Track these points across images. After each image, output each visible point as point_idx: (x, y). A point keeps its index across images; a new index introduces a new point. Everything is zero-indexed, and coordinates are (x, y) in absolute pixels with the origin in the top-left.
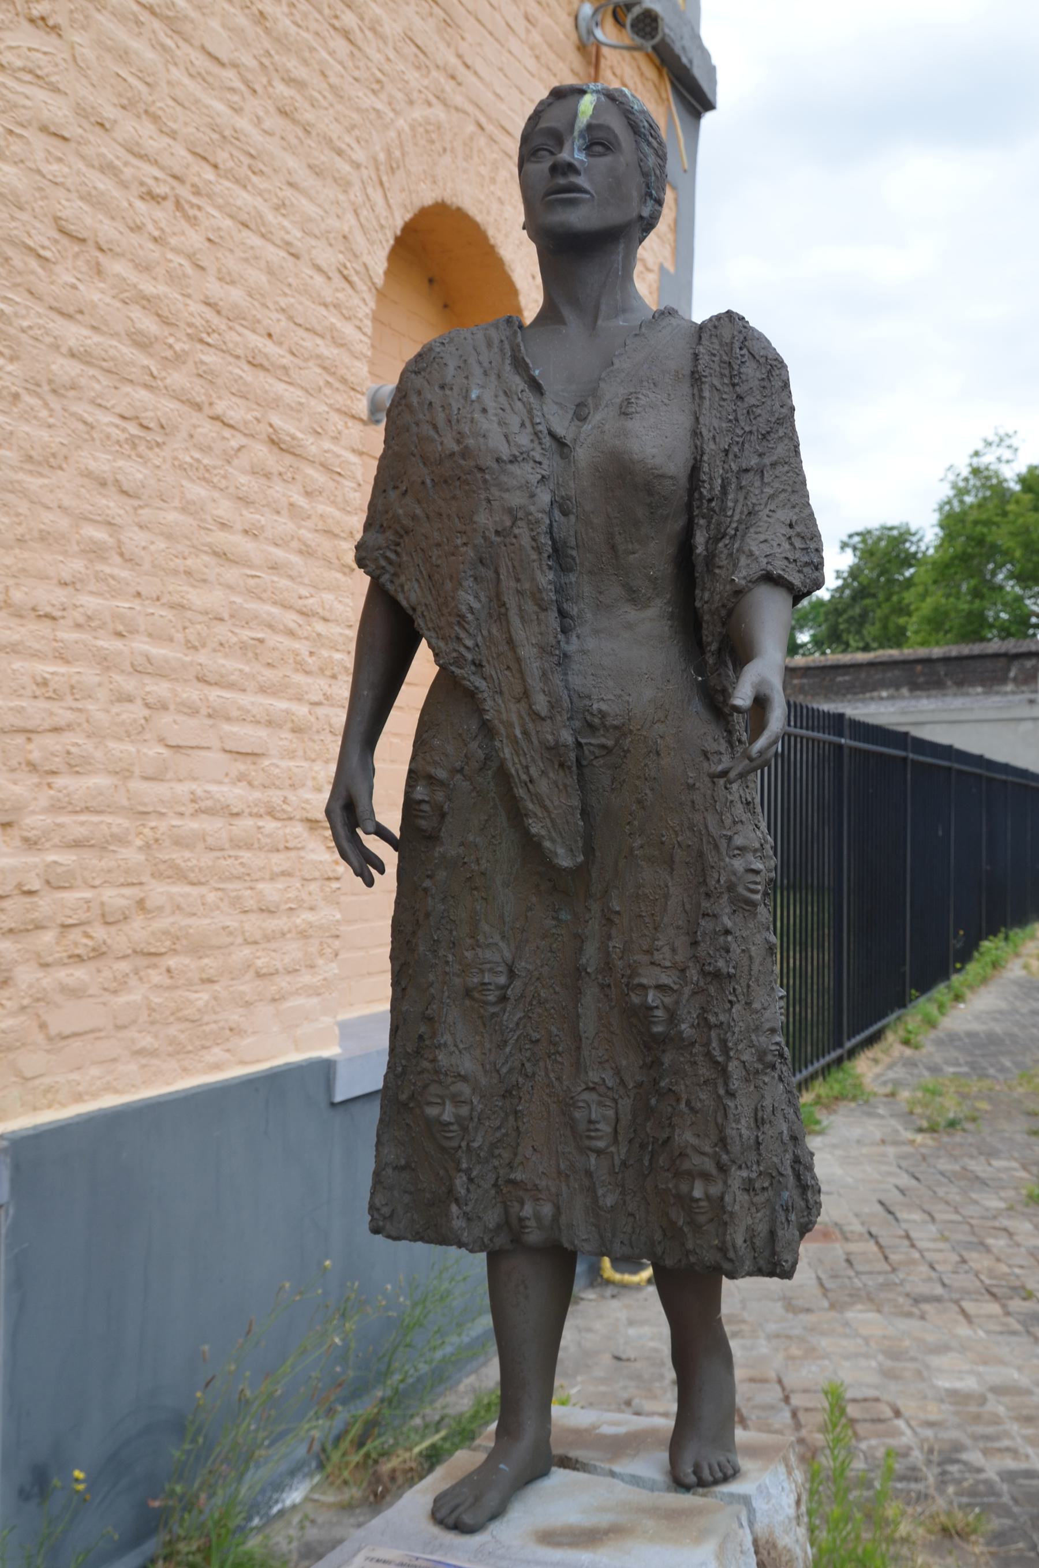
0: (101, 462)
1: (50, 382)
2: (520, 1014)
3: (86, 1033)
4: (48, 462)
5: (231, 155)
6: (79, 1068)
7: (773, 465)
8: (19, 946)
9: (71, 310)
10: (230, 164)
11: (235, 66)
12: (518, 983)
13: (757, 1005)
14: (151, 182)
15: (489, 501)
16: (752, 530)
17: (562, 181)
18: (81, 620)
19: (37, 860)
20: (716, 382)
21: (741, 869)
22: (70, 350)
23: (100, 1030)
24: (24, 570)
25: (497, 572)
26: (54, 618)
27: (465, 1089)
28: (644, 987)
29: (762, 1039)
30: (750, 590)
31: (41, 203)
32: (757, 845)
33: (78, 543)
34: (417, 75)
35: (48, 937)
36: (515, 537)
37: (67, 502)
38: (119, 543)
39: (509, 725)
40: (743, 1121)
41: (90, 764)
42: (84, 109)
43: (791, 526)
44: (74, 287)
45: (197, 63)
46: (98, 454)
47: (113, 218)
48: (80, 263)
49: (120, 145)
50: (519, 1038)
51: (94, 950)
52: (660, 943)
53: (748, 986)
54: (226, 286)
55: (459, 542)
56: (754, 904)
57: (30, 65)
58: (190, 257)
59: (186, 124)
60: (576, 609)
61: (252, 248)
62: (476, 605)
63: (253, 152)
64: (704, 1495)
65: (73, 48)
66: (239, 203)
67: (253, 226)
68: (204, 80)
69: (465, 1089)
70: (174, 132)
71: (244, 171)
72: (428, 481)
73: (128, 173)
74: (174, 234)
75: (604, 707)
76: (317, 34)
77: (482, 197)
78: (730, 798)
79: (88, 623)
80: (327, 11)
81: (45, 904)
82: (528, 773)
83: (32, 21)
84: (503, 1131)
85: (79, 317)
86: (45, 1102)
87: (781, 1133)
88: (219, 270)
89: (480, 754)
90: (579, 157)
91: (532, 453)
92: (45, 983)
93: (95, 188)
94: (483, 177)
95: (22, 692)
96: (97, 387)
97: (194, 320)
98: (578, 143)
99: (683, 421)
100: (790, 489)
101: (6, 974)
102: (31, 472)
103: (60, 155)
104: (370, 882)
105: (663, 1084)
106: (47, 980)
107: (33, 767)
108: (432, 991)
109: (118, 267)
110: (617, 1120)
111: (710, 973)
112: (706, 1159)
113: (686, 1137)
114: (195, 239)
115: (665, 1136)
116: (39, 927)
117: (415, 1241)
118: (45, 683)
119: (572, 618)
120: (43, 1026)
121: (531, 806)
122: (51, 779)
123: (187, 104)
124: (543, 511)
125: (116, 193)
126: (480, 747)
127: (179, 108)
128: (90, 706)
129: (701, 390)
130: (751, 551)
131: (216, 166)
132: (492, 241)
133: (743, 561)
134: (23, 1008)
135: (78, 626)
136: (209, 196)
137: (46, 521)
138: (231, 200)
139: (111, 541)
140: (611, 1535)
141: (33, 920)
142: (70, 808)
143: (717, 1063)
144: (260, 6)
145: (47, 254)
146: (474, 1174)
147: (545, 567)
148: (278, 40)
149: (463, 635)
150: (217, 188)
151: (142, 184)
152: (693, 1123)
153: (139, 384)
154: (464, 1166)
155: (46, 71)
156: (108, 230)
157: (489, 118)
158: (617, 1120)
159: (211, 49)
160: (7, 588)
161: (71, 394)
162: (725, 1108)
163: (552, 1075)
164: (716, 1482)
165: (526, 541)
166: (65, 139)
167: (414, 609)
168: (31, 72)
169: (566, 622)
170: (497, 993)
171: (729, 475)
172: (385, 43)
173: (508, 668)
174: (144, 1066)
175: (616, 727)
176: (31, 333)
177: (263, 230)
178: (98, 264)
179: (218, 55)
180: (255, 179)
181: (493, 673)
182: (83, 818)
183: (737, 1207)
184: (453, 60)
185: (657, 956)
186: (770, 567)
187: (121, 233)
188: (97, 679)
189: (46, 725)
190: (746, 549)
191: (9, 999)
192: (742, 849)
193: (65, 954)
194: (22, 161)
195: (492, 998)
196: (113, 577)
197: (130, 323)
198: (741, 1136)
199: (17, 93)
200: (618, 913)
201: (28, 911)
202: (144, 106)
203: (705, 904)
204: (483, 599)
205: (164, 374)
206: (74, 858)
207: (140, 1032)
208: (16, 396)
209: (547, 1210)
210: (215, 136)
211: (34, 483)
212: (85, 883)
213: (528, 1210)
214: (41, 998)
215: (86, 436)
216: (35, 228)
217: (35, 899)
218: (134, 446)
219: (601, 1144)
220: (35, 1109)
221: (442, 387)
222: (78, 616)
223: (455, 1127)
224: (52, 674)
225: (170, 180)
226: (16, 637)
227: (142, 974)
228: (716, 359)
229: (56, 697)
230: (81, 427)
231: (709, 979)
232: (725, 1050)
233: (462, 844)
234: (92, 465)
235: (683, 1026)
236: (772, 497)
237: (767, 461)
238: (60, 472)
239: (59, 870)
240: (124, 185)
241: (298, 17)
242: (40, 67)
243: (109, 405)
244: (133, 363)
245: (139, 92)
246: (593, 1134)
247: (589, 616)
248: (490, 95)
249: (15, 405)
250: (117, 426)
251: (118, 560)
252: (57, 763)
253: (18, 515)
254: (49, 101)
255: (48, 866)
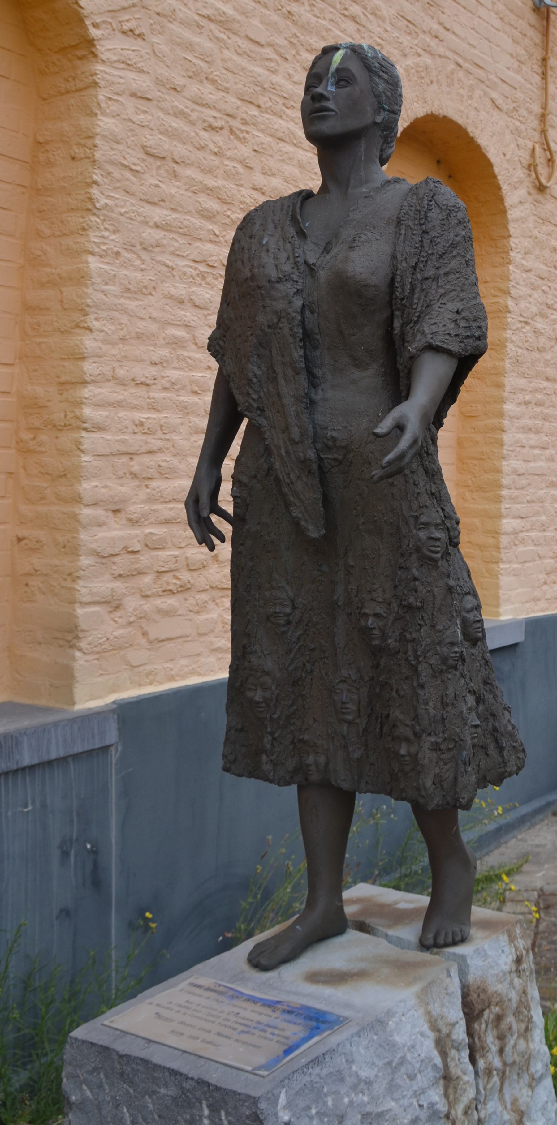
0: (180, 289)
1: (141, 243)
2: (300, 632)
3: (177, 638)
4: (141, 292)
5: (270, 99)
6: (172, 660)
7: (446, 274)
8: (127, 585)
9: (156, 200)
10: (270, 104)
11: (271, 45)
12: (298, 613)
13: (440, 627)
14: (211, 120)
15: (264, 307)
16: (427, 317)
17: (317, 105)
18: (167, 385)
19: (138, 532)
20: (411, 224)
21: (425, 538)
22: (155, 223)
23: (187, 637)
24: (126, 357)
25: (271, 351)
26: (148, 385)
27: (267, 679)
28: (367, 615)
29: (445, 649)
30: (419, 356)
31: (133, 138)
32: (439, 521)
33: (164, 339)
34: (409, 38)
35: (148, 579)
36: (280, 329)
37: (155, 314)
38: (194, 337)
39: (278, 448)
40: (431, 704)
41: (176, 472)
42: (161, 81)
43: (458, 312)
44: (157, 186)
45: (243, 46)
46: (177, 285)
47: (184, 143)
48: (162, 171)
49: (188, 99)
50: (299, 648)
51: (181, 586)
52: (375, 586)
53: (433, 614)
54: (268, 177)
55: (249, 333)
56: (436, 561)
57: (122, 58)
58: (242, 162)
59: (236, 83)
60: (321, 372)
61: (287, 153)
62: (259, 373)
63: (285, 95)
64: (437, 954)
65: (153, 46)
66: (276, 127)
67: (287, 140)
68: (248, 56)
69: (267, 679)
70: (227, 89)
71: (280, 107)
72: (237, 297)
73: (194, 116)
74: (229, 149)
75: (335, 434)
76: (332, 20)
77: (462, 108)
78: (417, 491)
79: (173, 386)
80: (338, 6)
81: (145, 559)
82: (289, 478)
83: (124, 33)
84: (295, 707)
85: (162, 203)
86: (148, 681)
87: (462, 712)
88: (263, 168)
89: (265, 466)
90: (331, 88)
91: (292, 276)
92: (145, 607)
93: (171, 126)
94: (462, 96)
95: (125, 430)
96: (176, 244)
97: (245, 200)
98: (332, 80)
99: (388, 249)
100: (459, 289)
101: (118, 602)
102: (129, 298)
103: (145, 109)
104: (212, 547)
105: (381, 679)
106: (148, 606)
107: (134, 475)
108: (249, 617)
109: (189, 172)
110: (359, 703)
111: (405, 606)
112: (408, 729)
113: (397, 714)
114: (244, 151)
115: (386, 713)
116: (141, 573)
117: (250, 777)
118: (142, 424)
119: (318, 378)
120: (145, 634)
121: (292, 499)
122: (147, 482)
123: (235, 71)
124: (296, 312)
125: (187, 128)
126: (265, 462)
127: (229, 74)
128: (175, 437)
129: (400, 229)
130: (423, 331)
131: (259, 106)
132: (471, 135)
133: (419, 336)
134: (130, 623)
135: (165, 389)
136: (254, 124)
137: (141, 326)
138: (271, 126)
139: (188, 336)
140: (355, 977)
141: (136, 569)
142: (162, 500)
143: (412, 665)
144: (288, 9)
145: (138, 168)
146: (276, 735)
147: (297, 347)
148: (303, 27)
149: (251, 391)
150: (260, 119)
151: (204, 121)
152: (400, 705)
153: (206, 241)
154: (269, 730)
155: (134, 61)
156: (180, 150)
157: (465, 59)
158: (359, 703)
159: (252, 37)
160: (114, 369)
161: (157, 250)
162: (417, 694)
163: (323, 672)
164: (446, 945)
165: (286, 331)
166: (148, 99)
167: (229, 376)
168: (123, 62)
169: (313, 381)
170: (285, 618)
171: (416, 282)
172: (384, 21)
173: (278, 412)
174: (220, 659)
175: (343, 447)
176: (127, 215)
177: (295, 141)
178: (174, 171)
179: (257, 40)
180: (288, 111)
181: (270, 415)
182: (171, 505)
183: (426, 761)
184: (436, 26)
185: (374, 595)
186: (431, 341)
187: (190, 152)
188: (179, 421)
189: (143, 450)
190: (421, 329)
191: (120, 617)
192: (427, 525)
193: (160, 590)
194: (118, 115)
195: (282, 622)
196: (190, 358)
197: (198, 205)
198: (429, 714)
199: (114, 75)
200: (352, 567)
201: (133, 563)
202: (205, 76)
203: (401, 561)
204: (263, 368)
205: (224, 233)
206: (166, 530)
207: (217, 637)
208: (118, 254)
209: (322, 760)
210: (258, 89)
211: (131, 304)
212: (174, 545)
213: (310, 759)
214: (144, 617)
215: (169, 274)
216: (128, 154)
217: (138, 556)
218: (204, 278)
219: (350, 717)
220: (140, 685)
221: (251, 237)
222: (165, 383)
223: (263, 705)
224: (147, 418)
225: (225, 117)
226: (121, 397)
227: (218, 601)
228: (413, 209)
229: (150, 432)
230: (164, 269)
231: (405, 610)
232: (417, 657)
233: (259, 523)
234: (173, 291)
235: (390, 641)
236: (443, 295)
237: (441, 272)
238: (150, 297)
239: (154, 538)
240: (192, 123)
241: (317, 12)
242: (129, 59)
243: (184, 255)
244: (201, 229)
245: (201, 67)
246: (344, 711)
247: (329, 376)
248: (465, 45)
249: (117, 259)
250: (191, 267)
251: (194, 347)
252: (152, 472)
253: (120, 324)
254: (136, 78)
255: (146, 535)
